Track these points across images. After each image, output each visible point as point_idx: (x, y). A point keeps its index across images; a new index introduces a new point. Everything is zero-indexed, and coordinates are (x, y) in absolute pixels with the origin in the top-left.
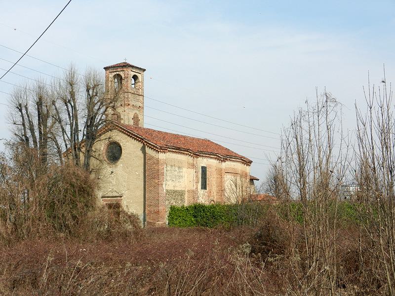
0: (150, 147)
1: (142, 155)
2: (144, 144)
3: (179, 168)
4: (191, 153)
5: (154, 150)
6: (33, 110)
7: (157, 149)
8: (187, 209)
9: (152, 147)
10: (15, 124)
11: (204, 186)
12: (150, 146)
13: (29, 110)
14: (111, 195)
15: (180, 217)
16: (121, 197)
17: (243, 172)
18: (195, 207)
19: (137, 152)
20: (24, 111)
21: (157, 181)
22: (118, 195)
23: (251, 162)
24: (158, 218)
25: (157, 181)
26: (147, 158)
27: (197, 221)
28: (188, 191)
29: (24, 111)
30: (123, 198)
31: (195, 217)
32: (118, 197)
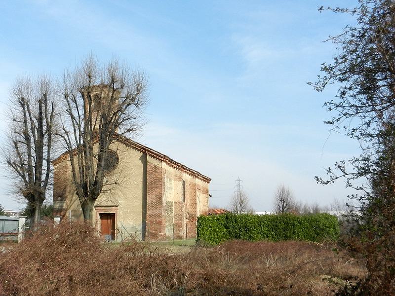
0: (152, 156)
1: (141, 165)
2: (144, 153)
3: (170, 179)
4: (179, 166)
5: (155, 157)
6: (34, 108)
7: (160, 158)
8: (218, 219)
9: (155, 156)
10: (15, 121)
11: (184, 201)
12: (152, 155)
13: (31, 108)
14: (106, 205)
15: (211, 227)
16: (117, 206)
17: (204, 188)
18: (227, 218)
19: (135, 161)
20: (26, 107)
21: (159, 191)
22: (114, 205)
23: (210, 180)
24: (160, 229)
25: (159, 191)
26: (148, 167)
27: (230, 233)
28: (176, 203)
29: (26, 107)
30: (118, 207)
31: (227, 228)
32: (113, 206)
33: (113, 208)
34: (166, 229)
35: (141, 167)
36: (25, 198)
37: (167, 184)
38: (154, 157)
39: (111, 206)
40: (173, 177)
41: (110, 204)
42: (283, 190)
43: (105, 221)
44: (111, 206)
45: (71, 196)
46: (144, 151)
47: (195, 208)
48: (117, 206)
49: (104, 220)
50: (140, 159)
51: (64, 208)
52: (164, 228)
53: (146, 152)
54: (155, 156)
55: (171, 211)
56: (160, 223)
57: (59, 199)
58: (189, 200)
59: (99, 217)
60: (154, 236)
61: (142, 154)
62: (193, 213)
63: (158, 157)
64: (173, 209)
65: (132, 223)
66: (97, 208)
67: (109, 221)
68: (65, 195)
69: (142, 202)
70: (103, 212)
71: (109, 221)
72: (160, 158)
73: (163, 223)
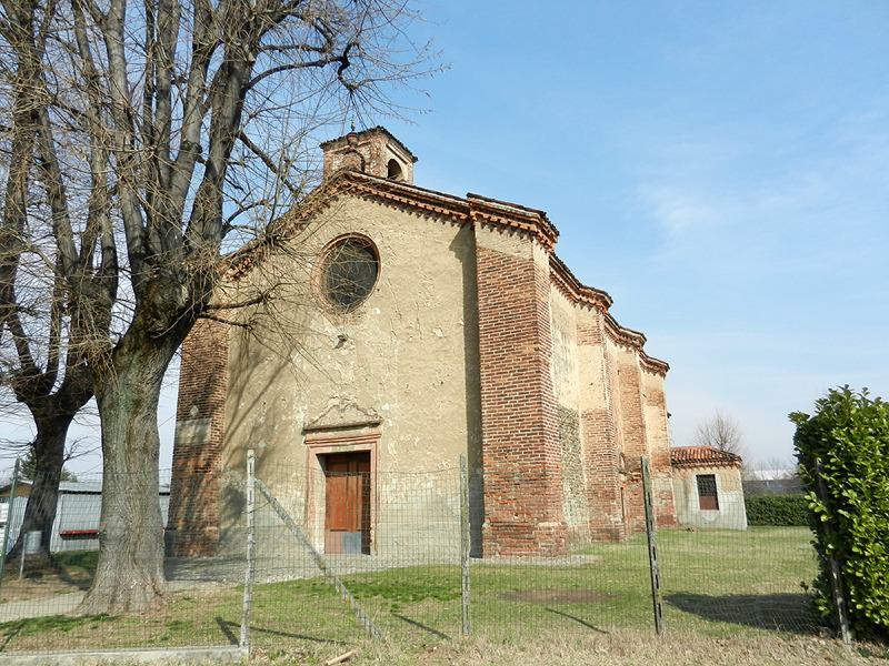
0: (493, 225)
1: (454, 265)
4: (588, 295)
7: (524, 226)
9: (504, 221)
12: (495, 218)
14: (339, 422)
16: (376, 425)
21: (528, 349)
22: (365, 419)
23: (667, 368)
28: (587, 416)
30: (381, 428)
32: (363, 425)
33: (365, 431)
34: (565, 507)
35: (458, 275)
36: (20, 399)
37: (556, 348)
38: (502, 227)
39: (354, 427)
40: (573, 331)
41: (352, 417)
42: (720, 425)
43: (339, 480)
44: (354, 427)
45: (235, 399)
46: (464, 216)
47: (642, 440)
48: (376, 425)
49: (334, 480)
50: (451, 248)
51: (206, 440)
52: (557, 503)
53: (466, 214)
54: (504, 221)
55: (575, 440)
56: (540, 479)
57: (194, 411)
58: (620, 417)
59: (317, 465)
60: (518, 534)
61: (457, 229)
62: (637, 455)
63: (515, 223)
64: (581, 437)
65: (429, 485)
66: (310, 436)
67: (355, 481)
68: (213, 399)
69: (464, 404)
70: (329, 450)
71: (353, 479)
72: (524, 226)
73: (552, 485)
